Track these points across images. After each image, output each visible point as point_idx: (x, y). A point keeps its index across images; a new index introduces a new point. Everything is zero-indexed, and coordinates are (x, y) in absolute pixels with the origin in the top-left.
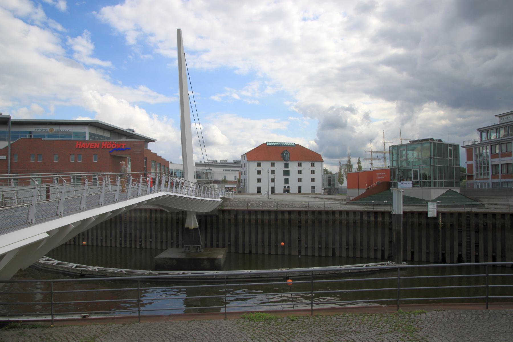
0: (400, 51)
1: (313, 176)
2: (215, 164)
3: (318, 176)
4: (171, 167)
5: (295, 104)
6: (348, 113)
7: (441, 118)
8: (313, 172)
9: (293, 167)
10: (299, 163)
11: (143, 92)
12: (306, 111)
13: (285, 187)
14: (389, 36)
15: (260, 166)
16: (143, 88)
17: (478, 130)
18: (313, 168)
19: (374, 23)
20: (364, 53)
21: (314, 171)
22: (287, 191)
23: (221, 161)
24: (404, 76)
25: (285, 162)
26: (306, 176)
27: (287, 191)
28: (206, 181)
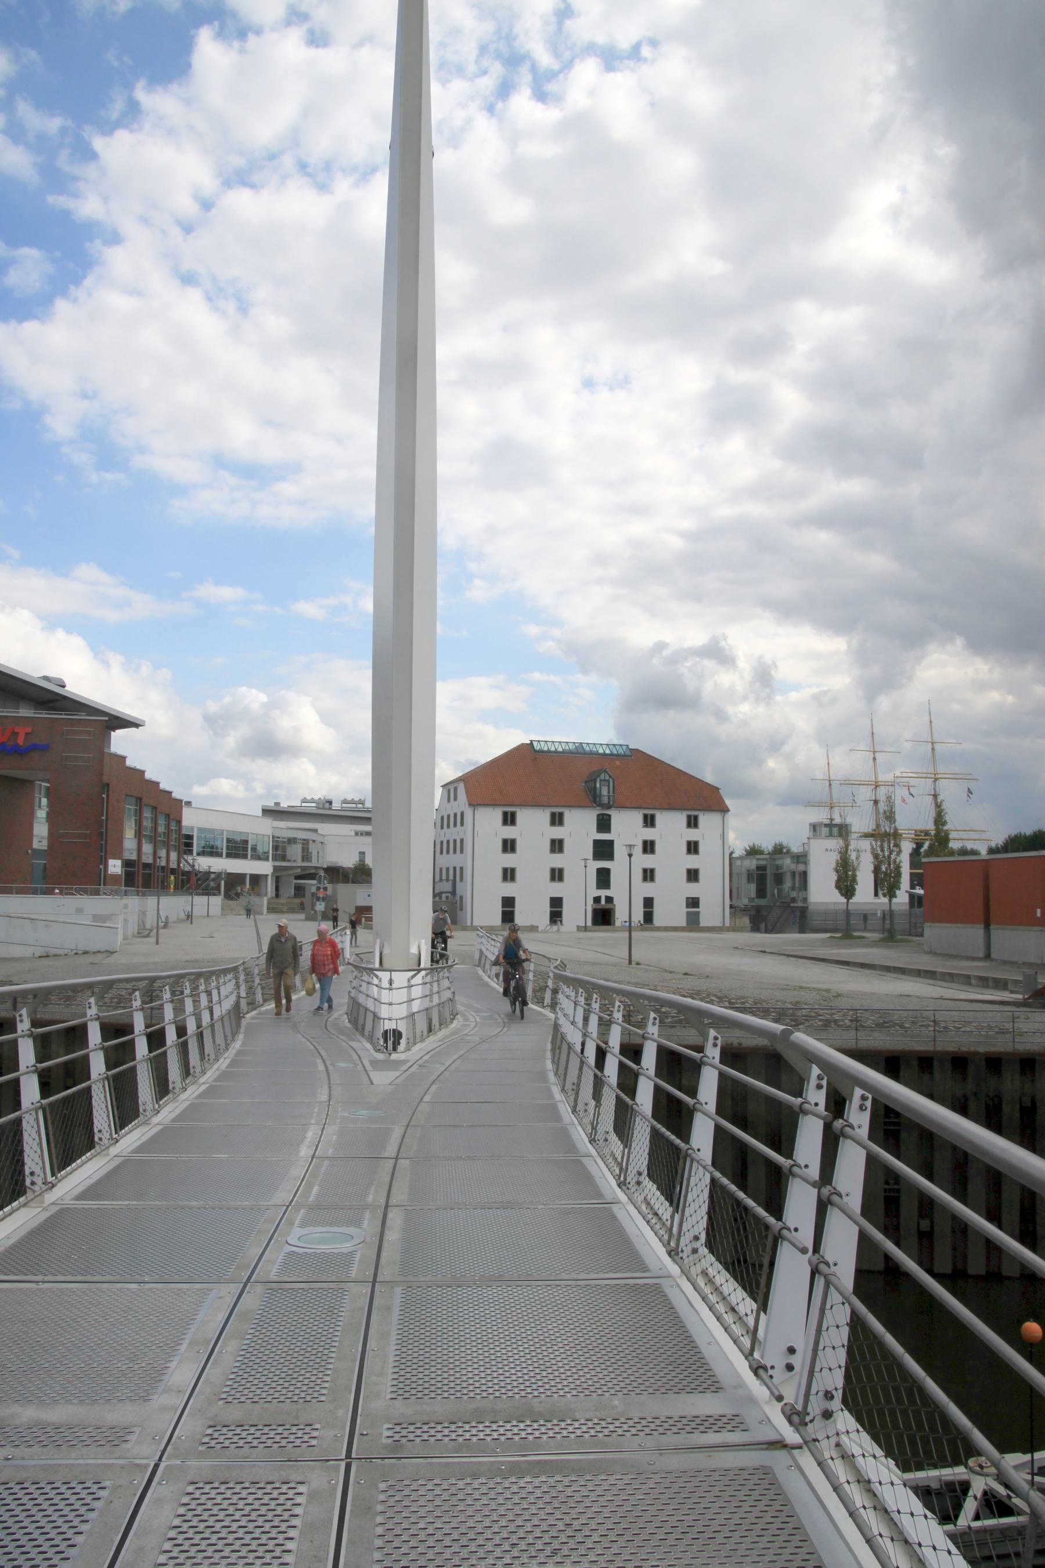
0: (855, 488)
1: (692, 861)
2: (324, 812)
3: (712, 865)
4: (190, 820)
5: (556, 632)
6: (709, 664)
7: (981, 686)
8: (693, 848)
9: (627, 827)
10: (645, 816)
11: (87, 584)
12: (584, 656)
13: (597, 900)
14: (830, 445)
15: (561, 823)
16: (87, 572)
18: (693, 835)
19: (792, 404)
20: (758, 491)
21: (696, 843)
22: (603, 916)
23: (345, 801)
24: (878, 562)
26: (671, 860)
27: (603, 916)
28: (303, 868)
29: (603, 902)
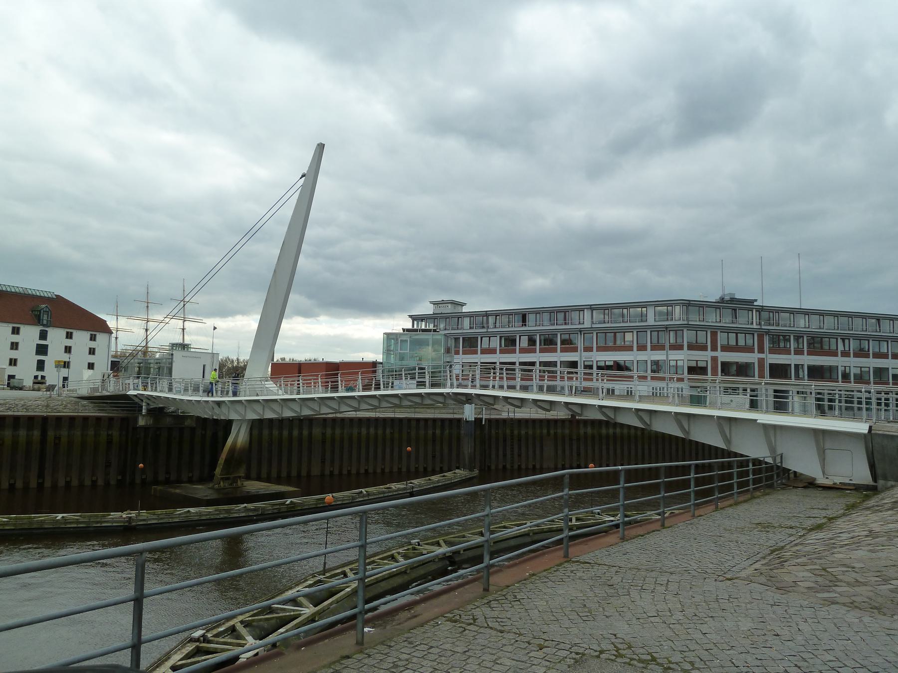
13: (36, 377)
17: (410, 316)
18: (93, 344)
25: (41, 328)
27: (39, 382)
29: (39, 378)
